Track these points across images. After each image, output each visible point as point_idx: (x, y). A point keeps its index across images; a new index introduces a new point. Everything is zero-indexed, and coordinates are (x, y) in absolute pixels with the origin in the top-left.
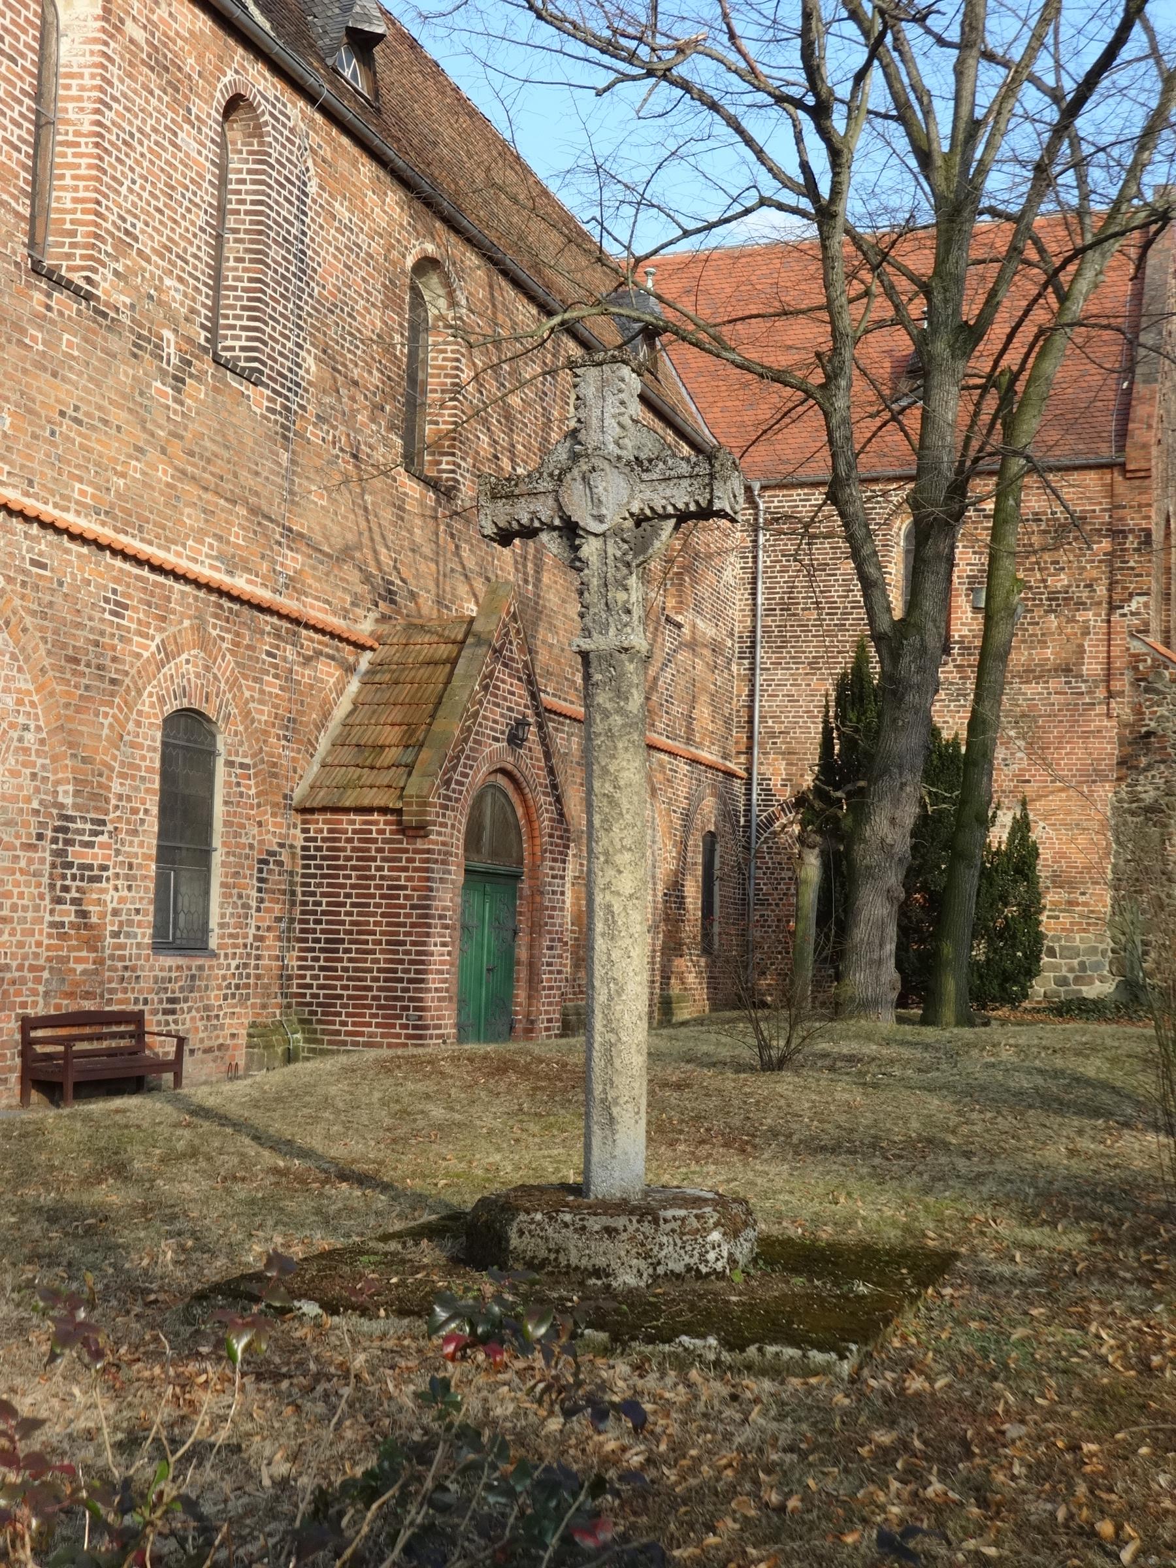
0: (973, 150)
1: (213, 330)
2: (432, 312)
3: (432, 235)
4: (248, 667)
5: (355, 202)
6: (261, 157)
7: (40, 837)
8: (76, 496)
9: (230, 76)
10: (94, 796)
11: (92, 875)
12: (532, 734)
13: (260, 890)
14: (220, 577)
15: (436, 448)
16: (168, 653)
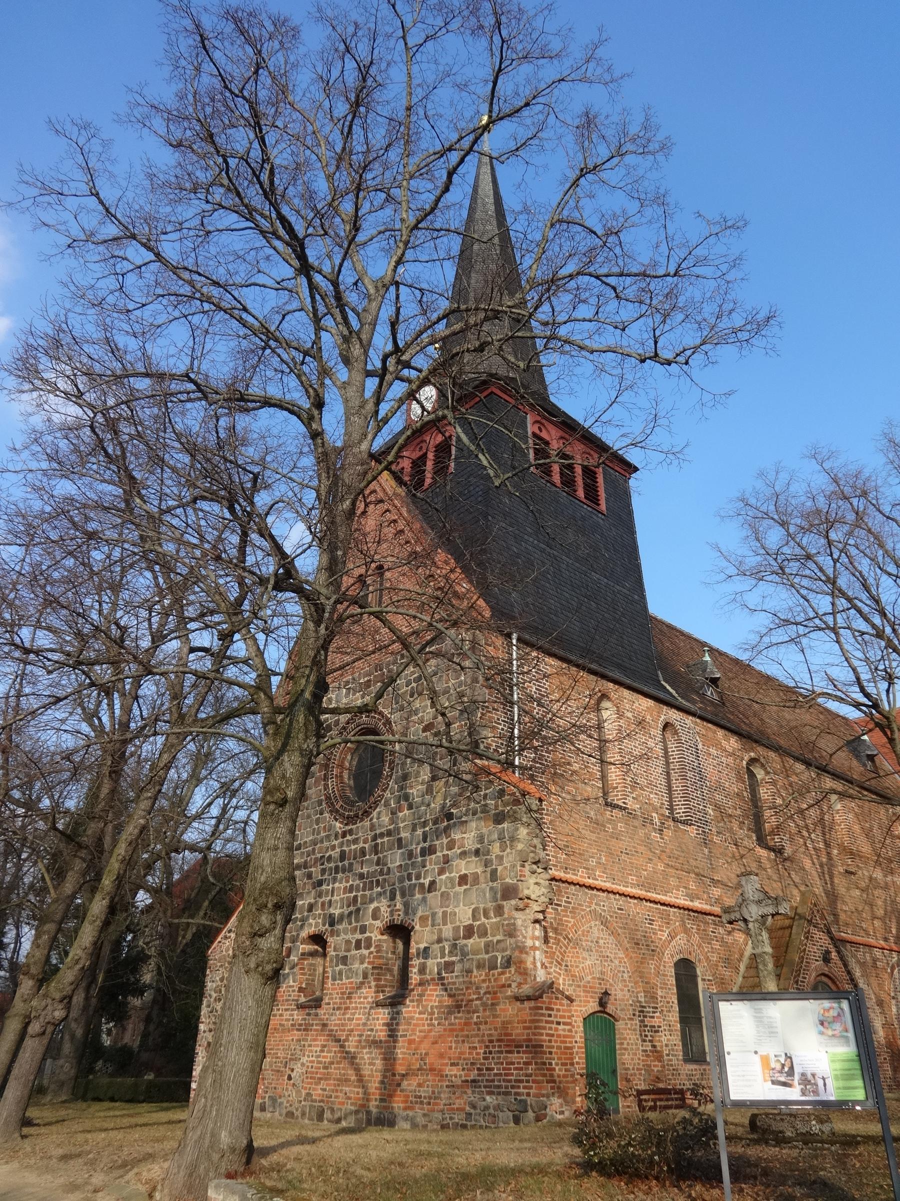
1: (671, 809)
2: (759, 777)
3: (752, 750)
4: (706, 938)
5: (718, 745)
6: (679, 741)
9: (663, 717)
10: (652, 997)
11: (655, 1030)
12: (834, 955)
14: (688, 903)
15: (772, 833)
16: (672, 937)
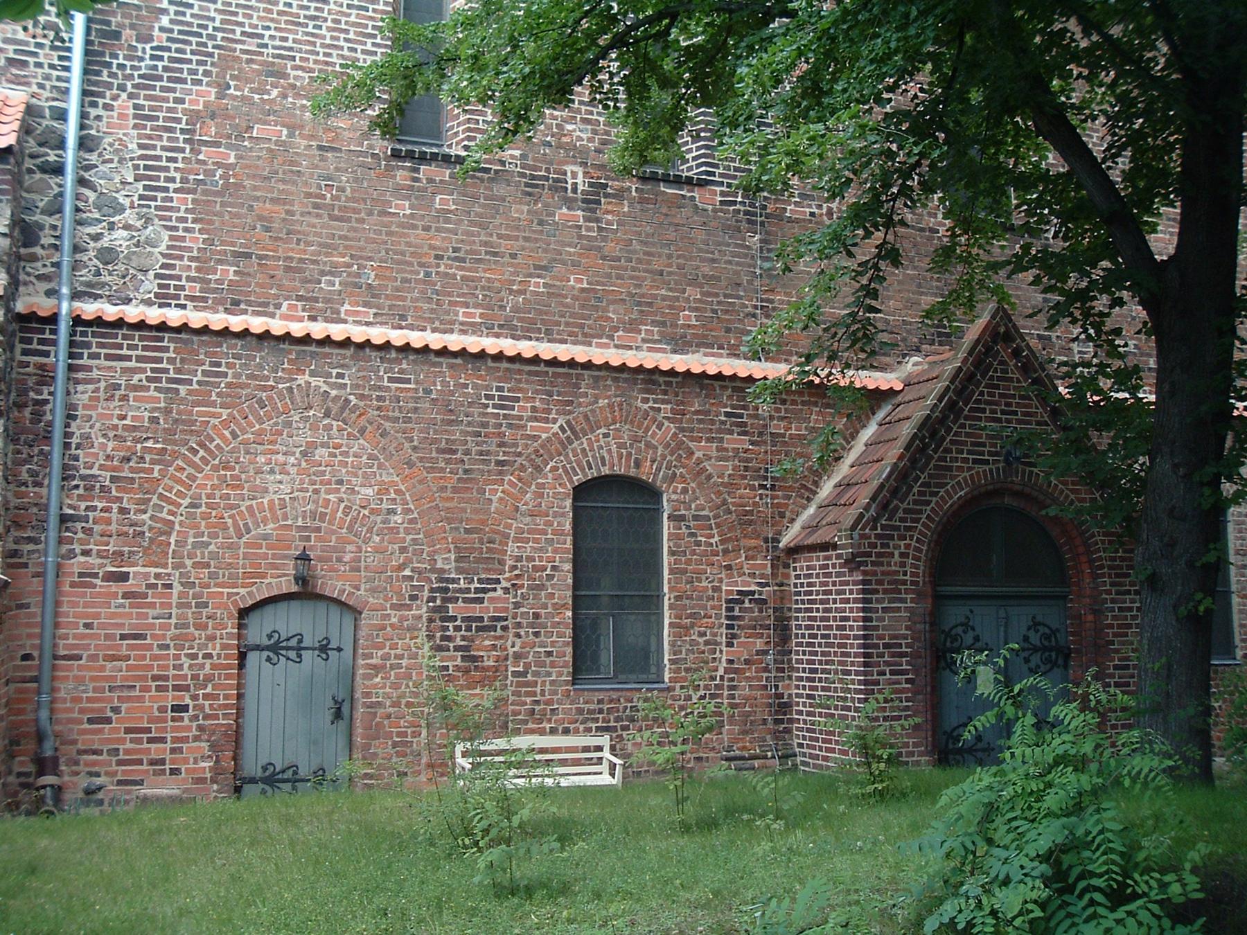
0: (813, 517)
7: (413, 598)
8: (461, 319)
13: (729, 627)
